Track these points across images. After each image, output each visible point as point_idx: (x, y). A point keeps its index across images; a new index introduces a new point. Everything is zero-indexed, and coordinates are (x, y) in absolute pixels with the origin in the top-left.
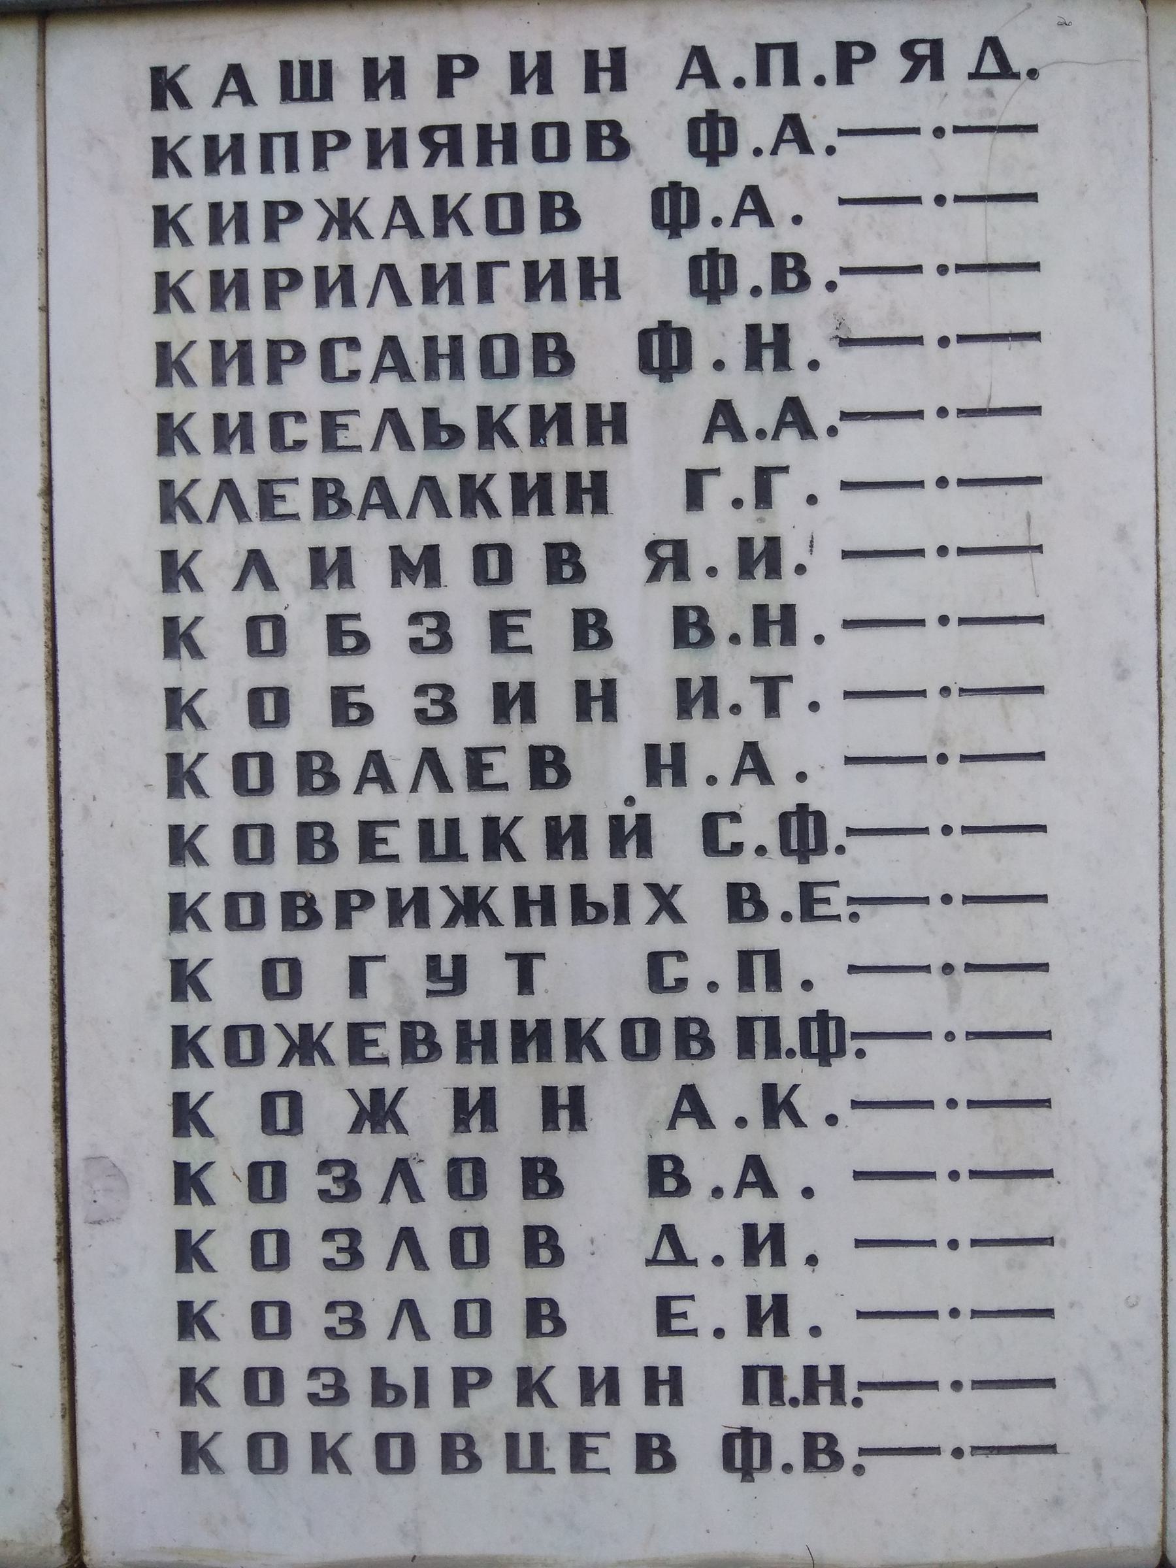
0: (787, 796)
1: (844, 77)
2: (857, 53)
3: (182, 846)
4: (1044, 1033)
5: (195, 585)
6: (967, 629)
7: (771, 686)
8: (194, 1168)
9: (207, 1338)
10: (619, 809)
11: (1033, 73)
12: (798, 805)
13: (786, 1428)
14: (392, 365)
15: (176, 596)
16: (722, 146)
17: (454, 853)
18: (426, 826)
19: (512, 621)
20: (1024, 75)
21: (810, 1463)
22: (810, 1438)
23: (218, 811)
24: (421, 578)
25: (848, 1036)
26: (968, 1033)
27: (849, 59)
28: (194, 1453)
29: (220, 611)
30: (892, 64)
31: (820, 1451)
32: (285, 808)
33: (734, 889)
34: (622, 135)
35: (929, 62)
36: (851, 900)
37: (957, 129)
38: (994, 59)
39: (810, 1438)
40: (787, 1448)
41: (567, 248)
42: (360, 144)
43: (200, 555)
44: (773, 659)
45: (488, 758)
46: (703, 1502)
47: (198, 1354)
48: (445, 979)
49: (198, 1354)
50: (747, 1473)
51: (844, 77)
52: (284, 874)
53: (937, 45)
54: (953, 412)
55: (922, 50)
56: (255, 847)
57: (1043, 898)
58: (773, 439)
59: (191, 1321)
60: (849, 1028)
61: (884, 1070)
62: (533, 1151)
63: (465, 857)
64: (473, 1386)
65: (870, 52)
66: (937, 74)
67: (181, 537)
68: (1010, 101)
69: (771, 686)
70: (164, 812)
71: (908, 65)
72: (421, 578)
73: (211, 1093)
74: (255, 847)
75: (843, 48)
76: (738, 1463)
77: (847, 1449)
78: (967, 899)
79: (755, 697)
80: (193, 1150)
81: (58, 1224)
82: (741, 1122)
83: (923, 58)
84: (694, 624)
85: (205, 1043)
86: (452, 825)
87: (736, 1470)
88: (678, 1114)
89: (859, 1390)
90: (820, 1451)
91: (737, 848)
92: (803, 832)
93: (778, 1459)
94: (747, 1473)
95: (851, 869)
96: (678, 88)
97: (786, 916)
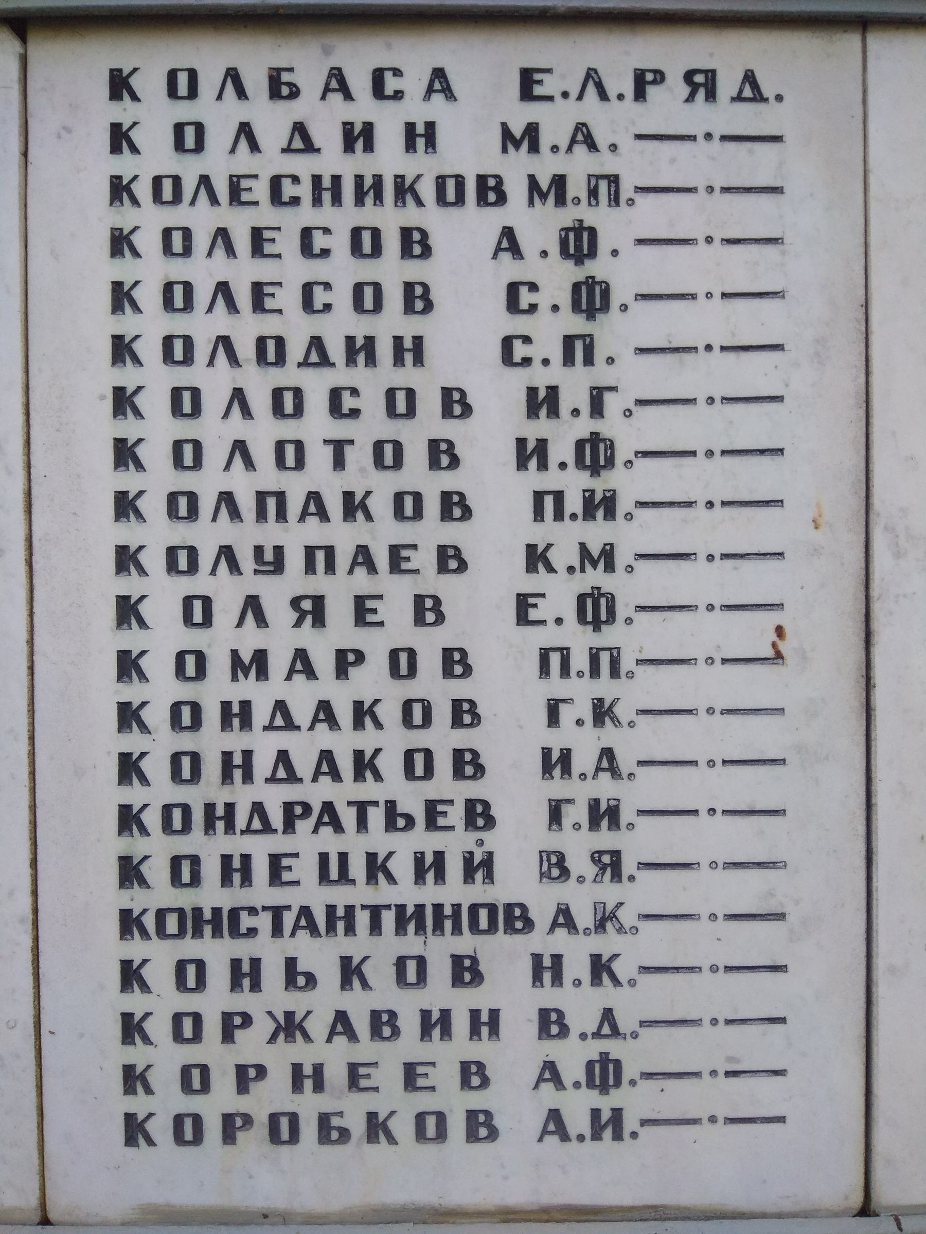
1: (640, 94)
3: (129, 768)
4: (778, 501)
5: (148, 1091)
8: (140, 1118)
9: (144, 1043)
12: (592, 433)
15: (121, 317)
17: (344, 877)
18: (324, 858)
23: (158, 745)
27: (643, 83)
28: (135, 1130)
32: (212, 741)
33: (544, 1014)
38: (751, 89)
43: (153, 1117)
45: (404, 553)
47: (139, 1104)
48: (269, 563)
49: (139, 1104)
51: (640, 94)
52: (210, 789)
53: (711, 75)
56: (190, 140)
58: (593, 778)
59: (133, 1079)
62: (488, 169)
63: (353, 882)
66: (711, 95)
67: (136, 949)
68: (746, 118)
70: (115, 744)
71: (295, 615)
72: (601, 565)
74: (190, 140)
80: (132, 639)
81: (30, 807)
83: (700, 85)
85: (146, 817)
86: (343, 858)
87: (589, 623)
95: (634, 1101)
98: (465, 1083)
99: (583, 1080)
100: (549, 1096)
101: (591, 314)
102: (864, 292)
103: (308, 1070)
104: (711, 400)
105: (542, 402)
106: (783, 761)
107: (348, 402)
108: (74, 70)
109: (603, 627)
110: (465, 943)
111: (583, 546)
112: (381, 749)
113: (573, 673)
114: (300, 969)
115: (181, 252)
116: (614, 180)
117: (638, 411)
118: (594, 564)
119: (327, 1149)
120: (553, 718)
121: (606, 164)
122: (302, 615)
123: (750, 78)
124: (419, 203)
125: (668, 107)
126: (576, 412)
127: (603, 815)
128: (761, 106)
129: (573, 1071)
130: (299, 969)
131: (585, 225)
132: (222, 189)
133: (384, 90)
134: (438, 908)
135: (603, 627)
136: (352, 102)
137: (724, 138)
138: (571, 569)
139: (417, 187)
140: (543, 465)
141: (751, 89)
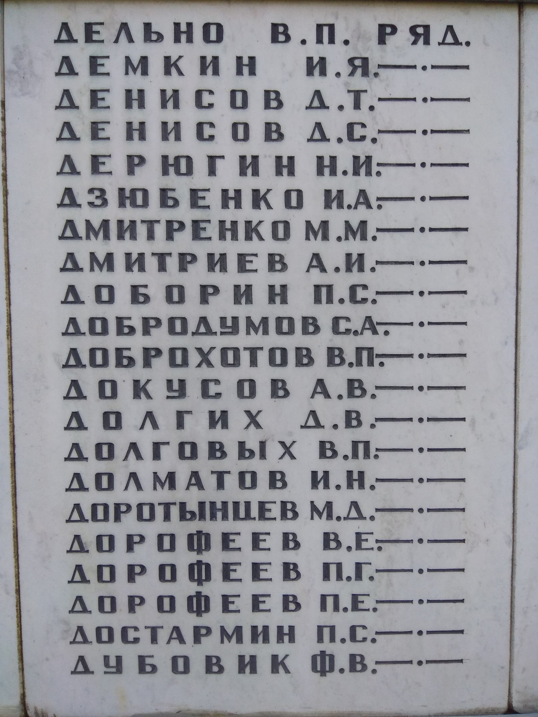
1: (382, 41)
6: (430, 513)
11: (468, 44)
13: (342, 653)
16: (327, 669)
20: (464, 43)
21: (353, 669)
22: (352, 657)
24: (358, 236)
25: (375, 324)
26: (427, 632)
27: (385, 32)
30: (403, 35)
31: (356, 663)
34: (287, 387)
35: (422, 37)
36: (377, 541)
39: (352, 657)
40: (342, 661)
42: (216, 633)
46: (302, 687)
48: (175, 391)
50: (323, 673)
51: (382, 41)
53: (427, 28)
58: (354, 209)
60: (376, 352)
61: (393, 372)
65: (394, 29)
66: (427, 42)
71: (413, 38)
72: (358, 236)
73: (261, 411)
75: (382, 27)
77: (370, 663)
78: (429, 450)
79: (348, 101)
84: (305, 356)
88: (310, 266)
89: (377, 264)
90: (356, 663)
92: (362, 449)
93: (337, 667)
94: (323, 673)
96: (125, 490)
97: (349, 548)
98: (286, 546)
105: (326, 450)
107: (207, 131)
108: (32, 31)
111: (347, 222)
112: (125, 490)
113: (339, 171)
114: (188, 509)
115: (169, 610)
116: (367, 444)
117: (378, 267)
118: (354, 235)
119: (184, 523)
123: (450, 29)
124: (261, 238)
125: (400, 47)
126: (345, 173)
128: (459, 47)
130: (188, 509)
134: (225, 517)
135: (328, 674)
138: (340, 140)
139: (285, 661)
140: (327, 486)
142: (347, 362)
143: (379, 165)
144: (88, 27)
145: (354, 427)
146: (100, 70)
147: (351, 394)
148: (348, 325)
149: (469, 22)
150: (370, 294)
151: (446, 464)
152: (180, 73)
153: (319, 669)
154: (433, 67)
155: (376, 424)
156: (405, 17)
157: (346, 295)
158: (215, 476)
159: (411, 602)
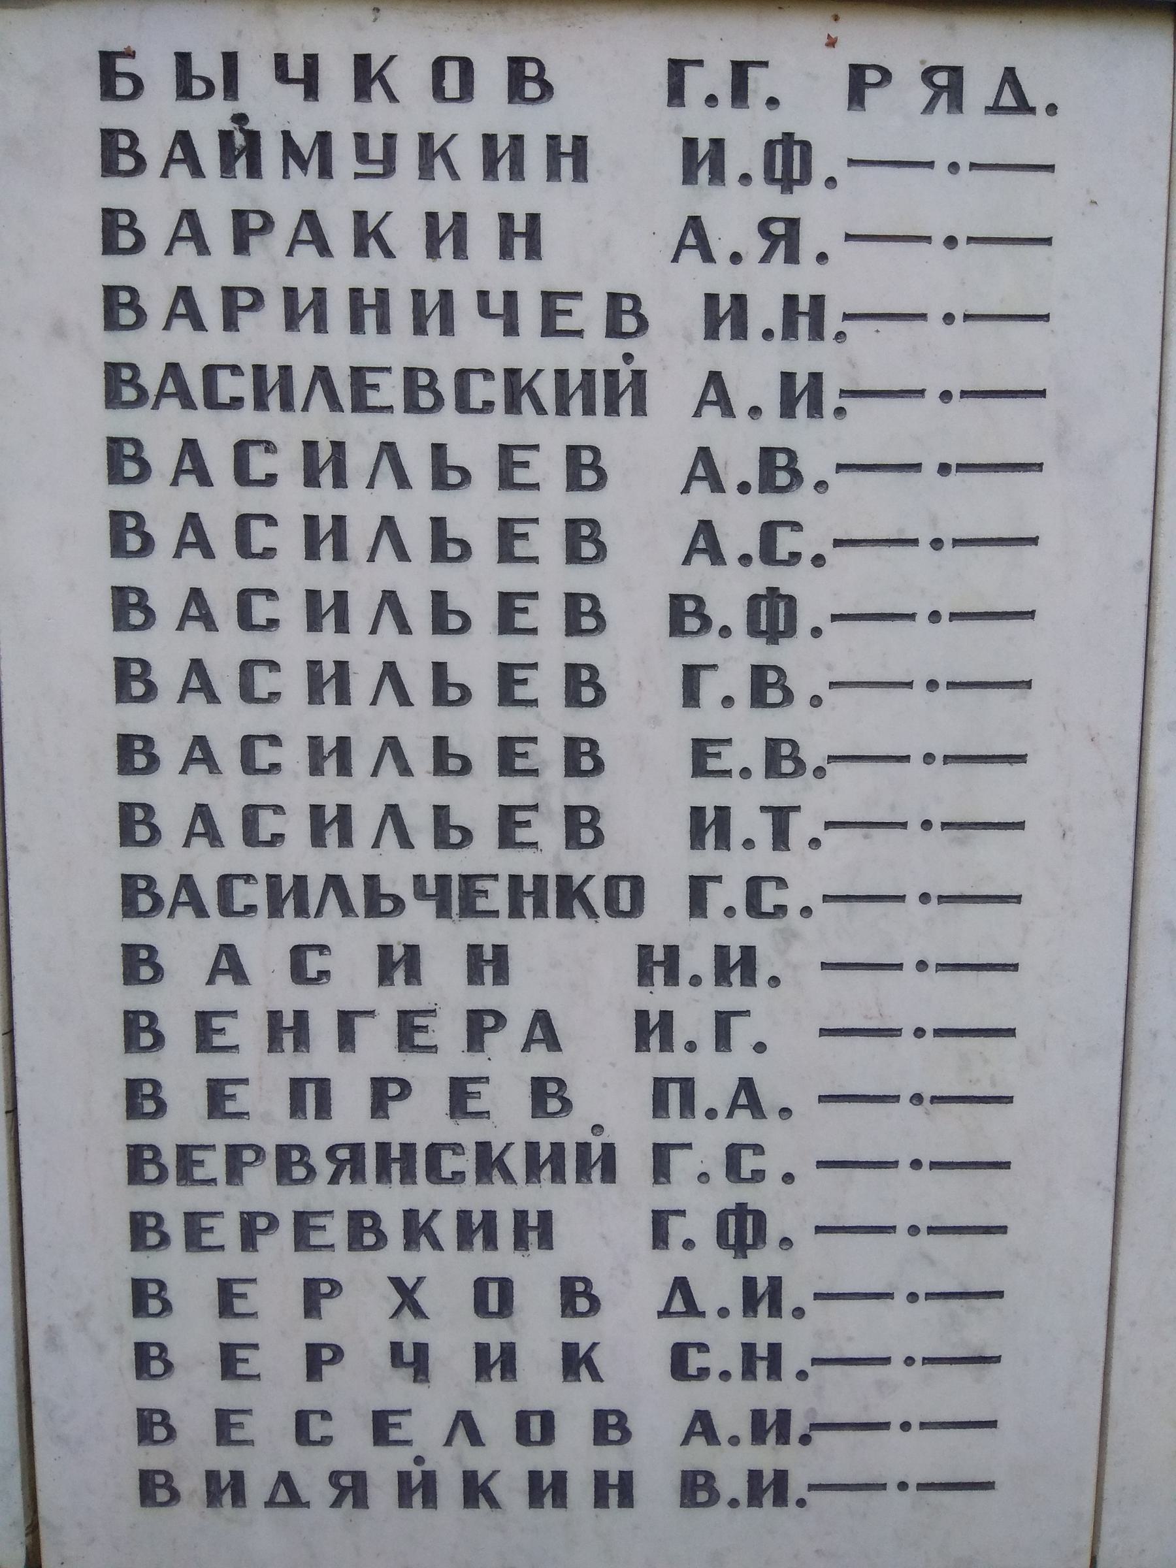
0: (774, 125)
2: (872, 76)
4: (1028, 613)
7: (780, 817)
10: (588, 1137)
11: (1052, 109)
12: (784, 134)
14: (715, 399)
19: (519, 674)
26: (962, 392)
28: (153, 1488)
29: (192, 1331)
31: (768, 1489)
35: (783, 243)
37: (964, 394)
38: (1013, 97)
39: (767, 454)
41: (534, 123)
44: (734, 996)
53: (956, 72)
54: (945, 617)
55: (941, 79)
57: (988, 1486)
64: (393, 1098)
66: (956, 104)
68: (1015, 137)
69: (780, 817)
71: (928, 93)
75: (857, 71)
76: (797, 150)
77: (812, 756)
78: (957, 542)
80: (155, 1395)
82: (704, 1177)
88: (692, 550)
91: (703, 1373)
99: (754, 549)
100: (702, 502)
101: (787, 184)
102: (1138, 735)
103: (331, 813)
104: (932, 685)
106: (1039, 467)
109: (796, 188)
110: (580, 428)
114: (300, 88)
120: (691, 697)
121: (804, 280)
122: (340, 1166)
127: (770, 1426)
129: (738, 464)
131: (797, 138)
132: (209, 895)
133: (469, 402)
135: (796, 188)
136: (424, 1321)
137: (886, 1426)
139: (536, 385)
141: (1013, 97)
142: (717, 625)
143: (847, 317)
144: (192, 1219)
145: (786, 775)
146: (473, 1105)
147: (768, 485)
148: (781, 897)
149: (1058, 55)
150: (806, 543)
151: (974, 936)
152: (388, 253)
153: (732, 1241)
154: (973, 166)
155: (828, 768)
156: (906, 44)
157: (753, 547)
158: (768, 818)
159: (901, 898)
